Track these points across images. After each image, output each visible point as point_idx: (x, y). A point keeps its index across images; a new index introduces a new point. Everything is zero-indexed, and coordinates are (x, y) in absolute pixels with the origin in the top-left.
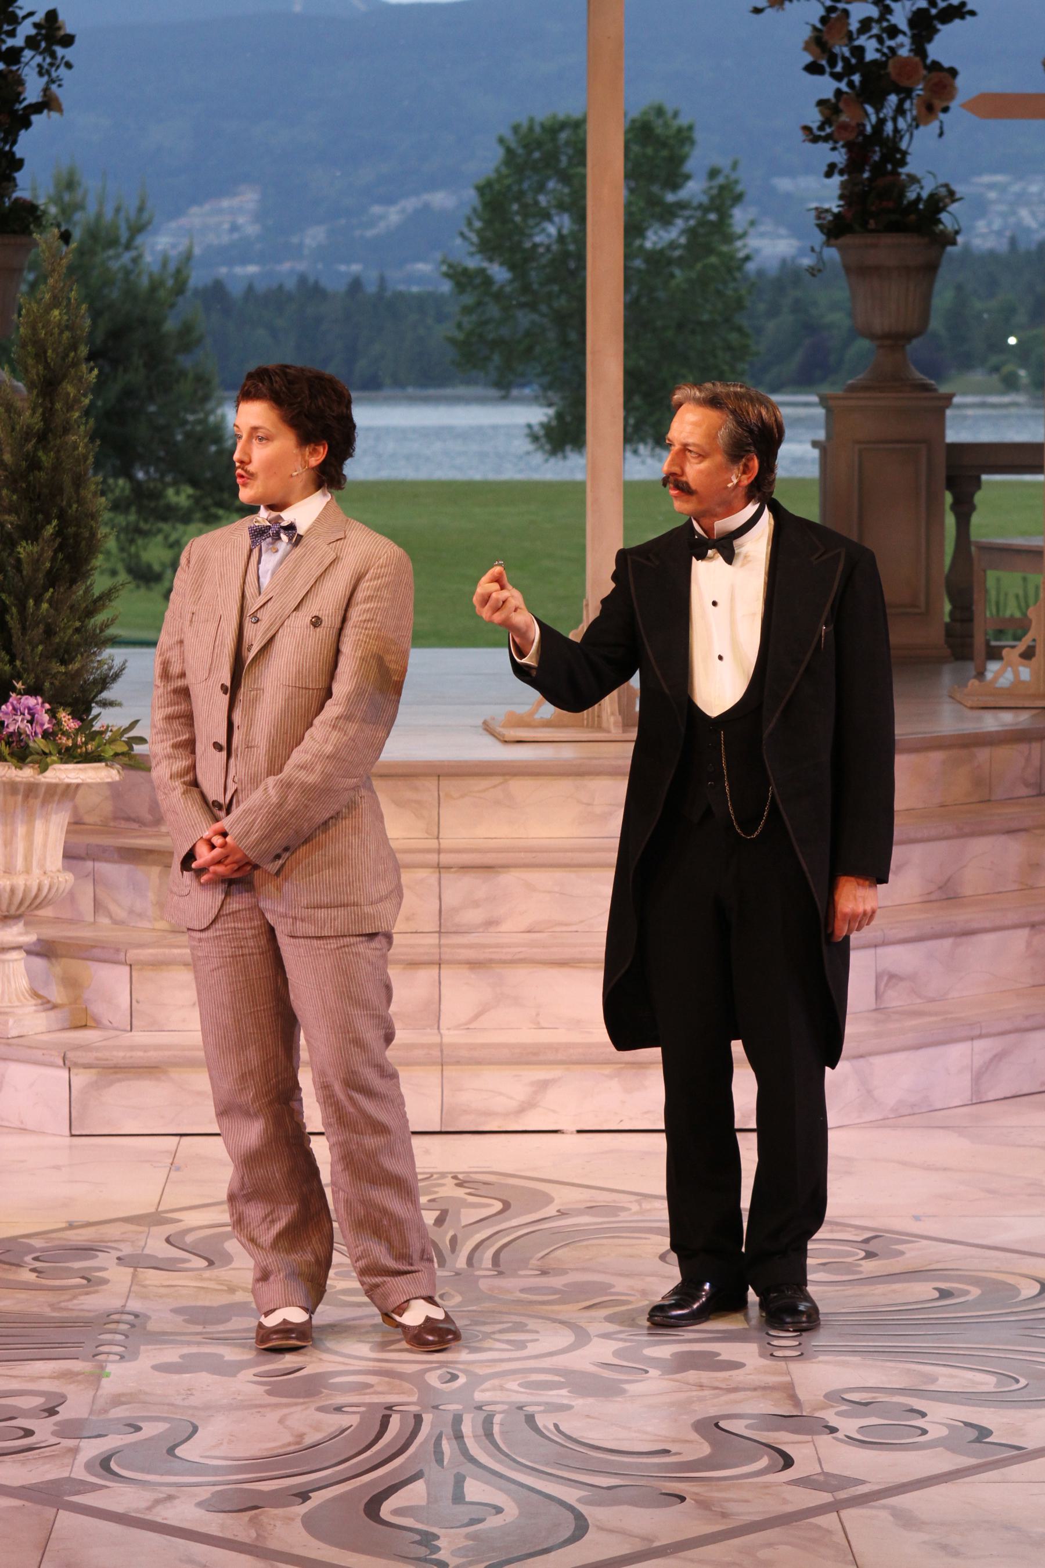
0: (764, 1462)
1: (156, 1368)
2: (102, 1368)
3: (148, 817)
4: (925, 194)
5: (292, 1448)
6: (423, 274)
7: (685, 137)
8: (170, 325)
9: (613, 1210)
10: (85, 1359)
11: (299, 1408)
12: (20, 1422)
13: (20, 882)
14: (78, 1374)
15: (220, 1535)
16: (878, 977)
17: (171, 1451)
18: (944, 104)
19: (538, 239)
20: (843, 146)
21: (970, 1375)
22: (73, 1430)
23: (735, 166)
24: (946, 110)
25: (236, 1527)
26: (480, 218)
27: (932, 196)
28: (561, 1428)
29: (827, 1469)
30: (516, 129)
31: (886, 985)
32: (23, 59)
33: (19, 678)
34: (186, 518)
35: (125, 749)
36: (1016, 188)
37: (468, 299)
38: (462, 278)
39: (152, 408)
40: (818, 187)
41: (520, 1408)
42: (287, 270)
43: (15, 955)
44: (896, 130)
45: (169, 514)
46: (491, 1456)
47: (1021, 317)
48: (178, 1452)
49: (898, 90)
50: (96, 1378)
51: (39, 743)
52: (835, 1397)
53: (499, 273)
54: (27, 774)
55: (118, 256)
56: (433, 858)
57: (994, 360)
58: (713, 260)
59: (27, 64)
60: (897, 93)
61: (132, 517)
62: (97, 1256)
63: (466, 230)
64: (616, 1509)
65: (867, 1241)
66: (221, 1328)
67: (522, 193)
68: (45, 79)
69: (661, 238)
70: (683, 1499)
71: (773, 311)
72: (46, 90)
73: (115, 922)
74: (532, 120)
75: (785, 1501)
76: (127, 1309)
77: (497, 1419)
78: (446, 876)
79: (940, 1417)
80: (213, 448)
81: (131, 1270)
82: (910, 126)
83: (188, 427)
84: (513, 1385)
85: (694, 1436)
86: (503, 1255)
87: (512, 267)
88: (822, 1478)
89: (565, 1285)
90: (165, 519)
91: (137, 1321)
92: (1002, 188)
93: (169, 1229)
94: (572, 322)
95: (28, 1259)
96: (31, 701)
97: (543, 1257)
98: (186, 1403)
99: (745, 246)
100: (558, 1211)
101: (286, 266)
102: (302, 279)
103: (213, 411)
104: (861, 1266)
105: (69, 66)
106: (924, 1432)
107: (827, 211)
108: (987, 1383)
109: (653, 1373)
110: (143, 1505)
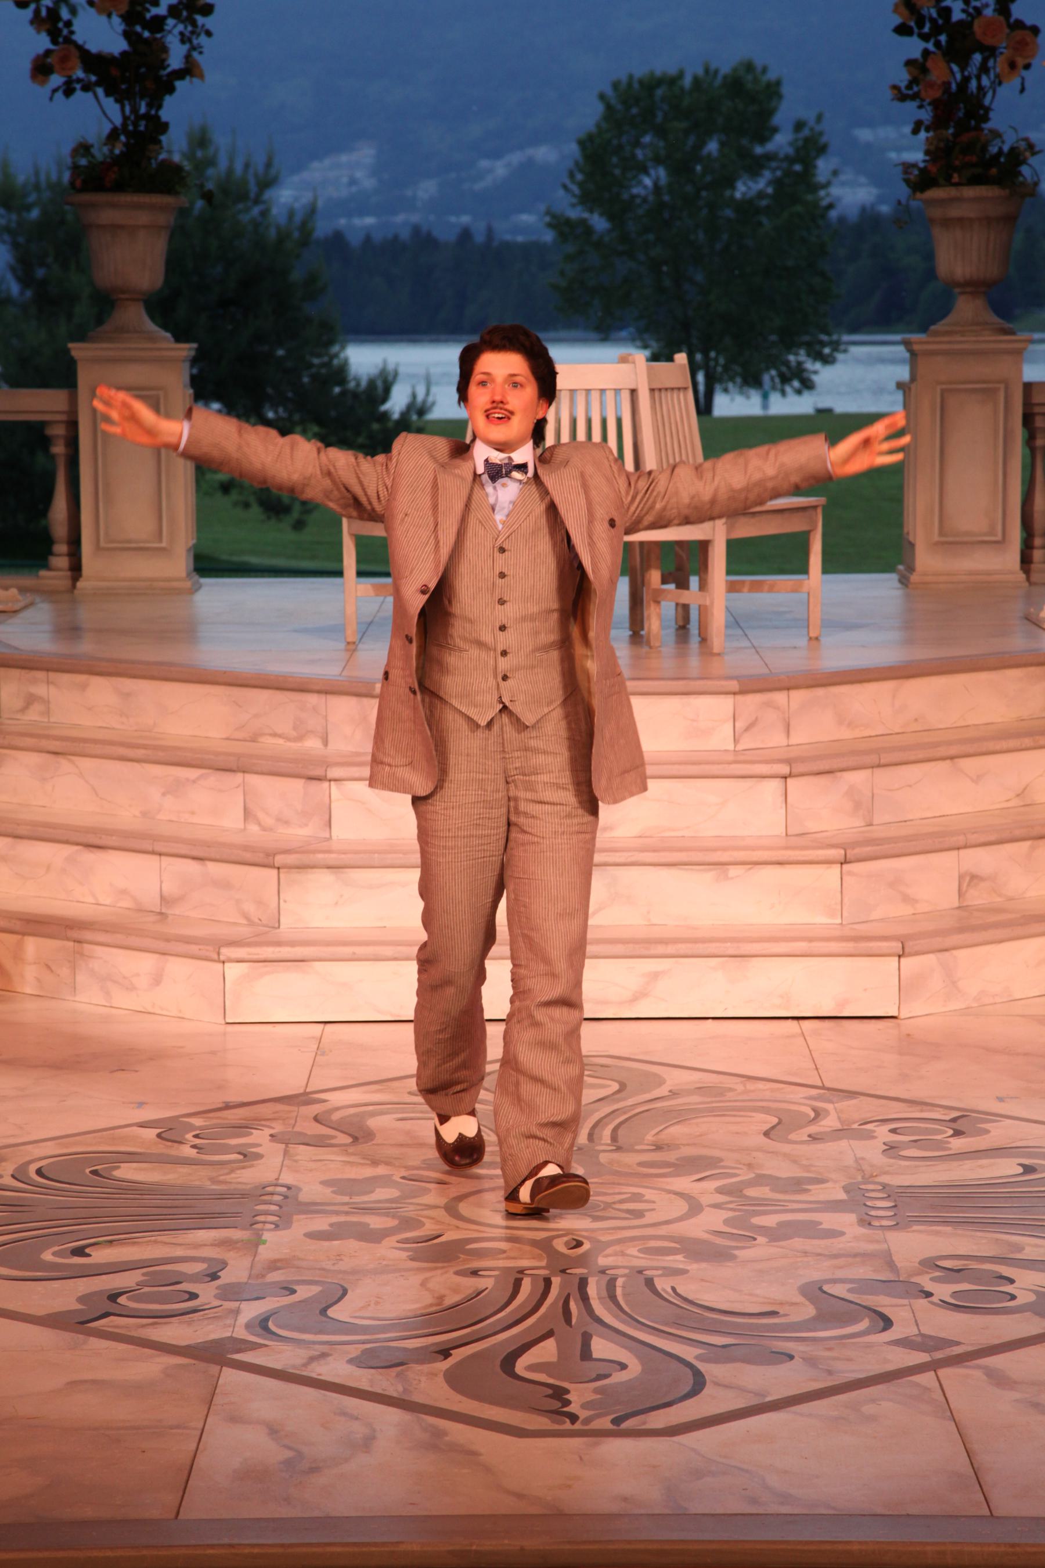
2: (260, 1236)
4: (1006, 148)
5: (434, 1309)
6: (528, 224)
7: (773, 90)
8: (297, 275)
9: (719, 1092)
10: (244, 1229)
11: (439, 1272)
12: (184, 1286)
14: (236, 1242)
15: (370, 1389)
16: (961, 878)
17: (324, 1312)
18: (1026, 61)
19: (635, 191)
20: (930, 104)
22: (233, 1293)
23: (819, 118)
24: (1027, 67)
25: (385, 1383)
26: (581, 171)
27: (1013, 149)
28: (678, 1291)
29: (925, 1330)
30: (616, 85)
31: (968, 885)
32: (167, 28)
37: (570, 248)
38: (562, 226)
39: (280, 352)
40: (902, 142)
41: (640, 1272)
42: (402, 221)
44: (980, 87)
46: (616, 1317)
48: (330, 1313)
49: (982, 48)
52: (930, 1264)
53: (599, 223)
55: (248, 210)
58: (799, 208)
59: (170, 32)
60: (982, 53)
62: (252, 1134)
63: (568, 182)
64: (730, 1366)
65: (954, 1120)
66: (366, 1198)
67: (620, 147)
68: (187, 46)
69: (749, 188)
70: (791, 1357)
72: (188, 57)
73: (264, 829)
74: (631, 77)
76: (281, 1182)
77: (620, 1282)
80: (337, 390)
81: (283, 1146)
82: (993, 83)
83: (314, 370)
84: (633, 1251)
85: (800, 1299)
86: (620, 1132)
87: (611, 217)
88: (919, 1339)
89: (677, 1159)
91: (289, 1193)
93: (316, 1109)
95: (189, 1136)
97: (657, 1134)
98: (336, 1268)
99: (828, 195)
100: (670, 1091)
101: (400, 218)
102: (416, 230)
103: (336, 355)
104: (949, 1143)
105: (209, 34)
106: (1013, 1297)
107: (914, 165)
110: (299, 1362)
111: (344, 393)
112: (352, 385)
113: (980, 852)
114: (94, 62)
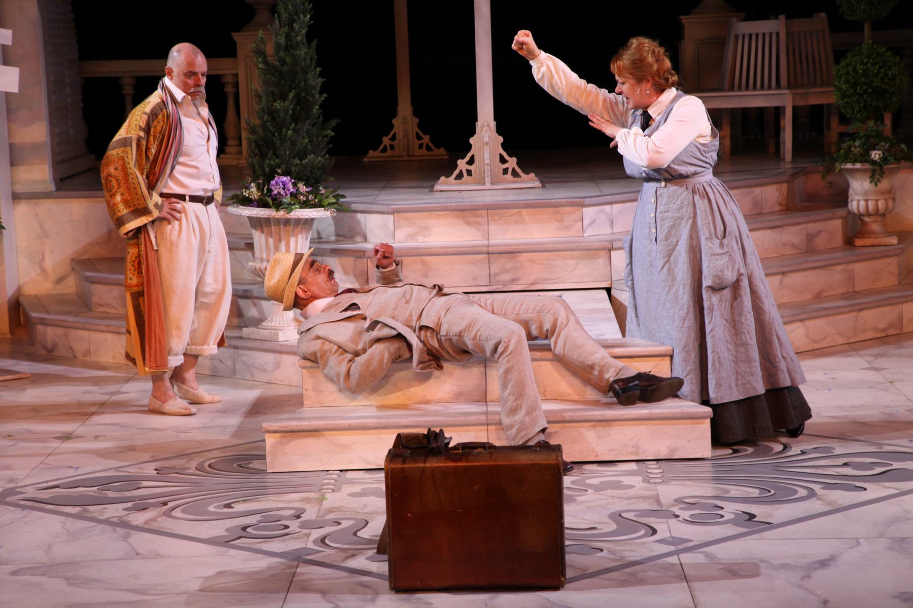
0: (642, 532)
1: (349, 495)
2: (323, 496)
3: (348, 234)
17: (355, 534)
21: (746, 489)
33: (279, 167)
35: (334, 200)
48: (359, 534)
50: (321, 500)
51: (287, 200)
52: (679, 501)
54: (281, 214)
75: (652, 551)
79: (730, 509)
96: (285, 179)
106: (722, 516)
108: (755, 493)
109: (590, 491)
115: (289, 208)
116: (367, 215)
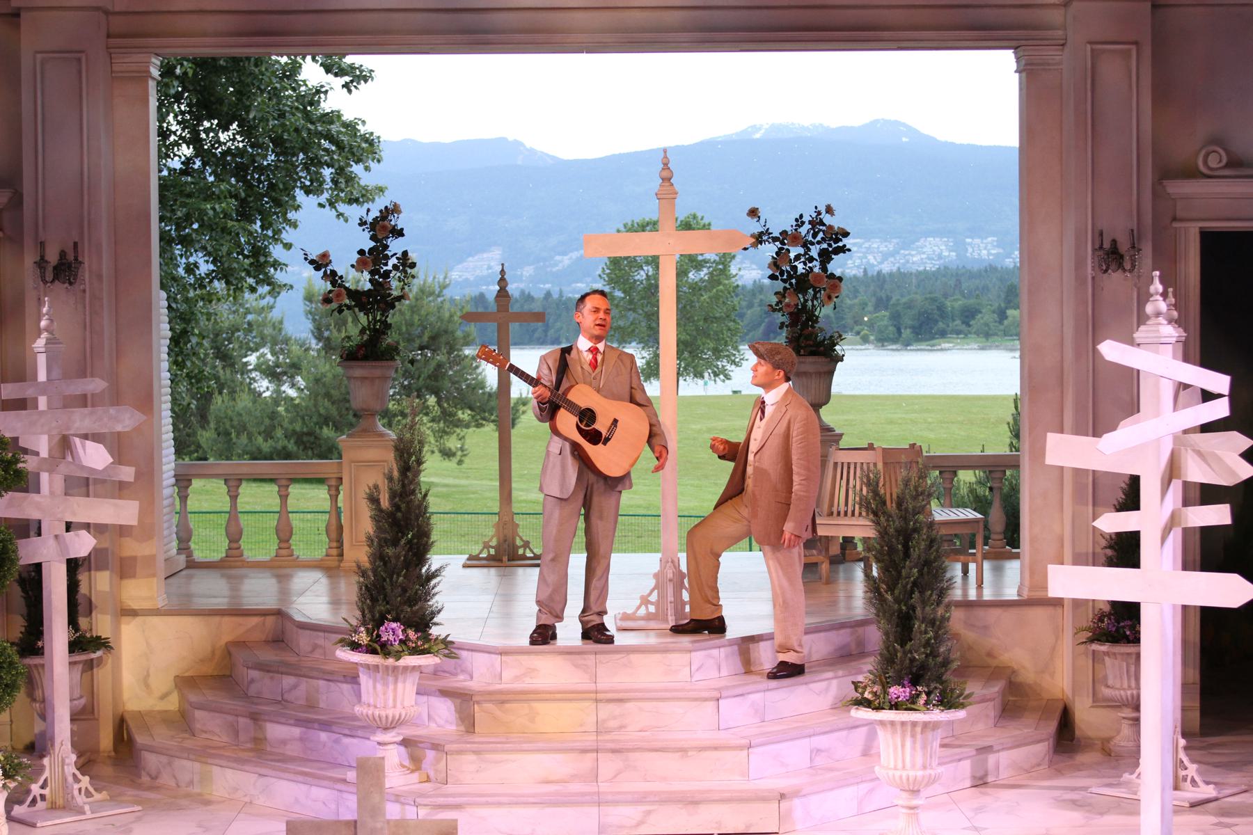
13: (390, 713)
33: (389, 612)
34: (467, 426)
36: (867, 245)
43: (391, 746)
44: (813, 305)
45: (459, 424)
47: (870, 308)
56: (593, 696)
57: (857, 328)
61: (442, 425)
71: (750, 306)
78: (600, 705)
87: (624, 292)
90: (457, 426)
92: (860, 246)
94: (653, 318)
96: (394, 625)
102: (523, 292)
111: (484, 393)
112: (488, 390)
113: (822, 737)
114: (354, 294)
115: (398, 656)
116: (475, 654)
